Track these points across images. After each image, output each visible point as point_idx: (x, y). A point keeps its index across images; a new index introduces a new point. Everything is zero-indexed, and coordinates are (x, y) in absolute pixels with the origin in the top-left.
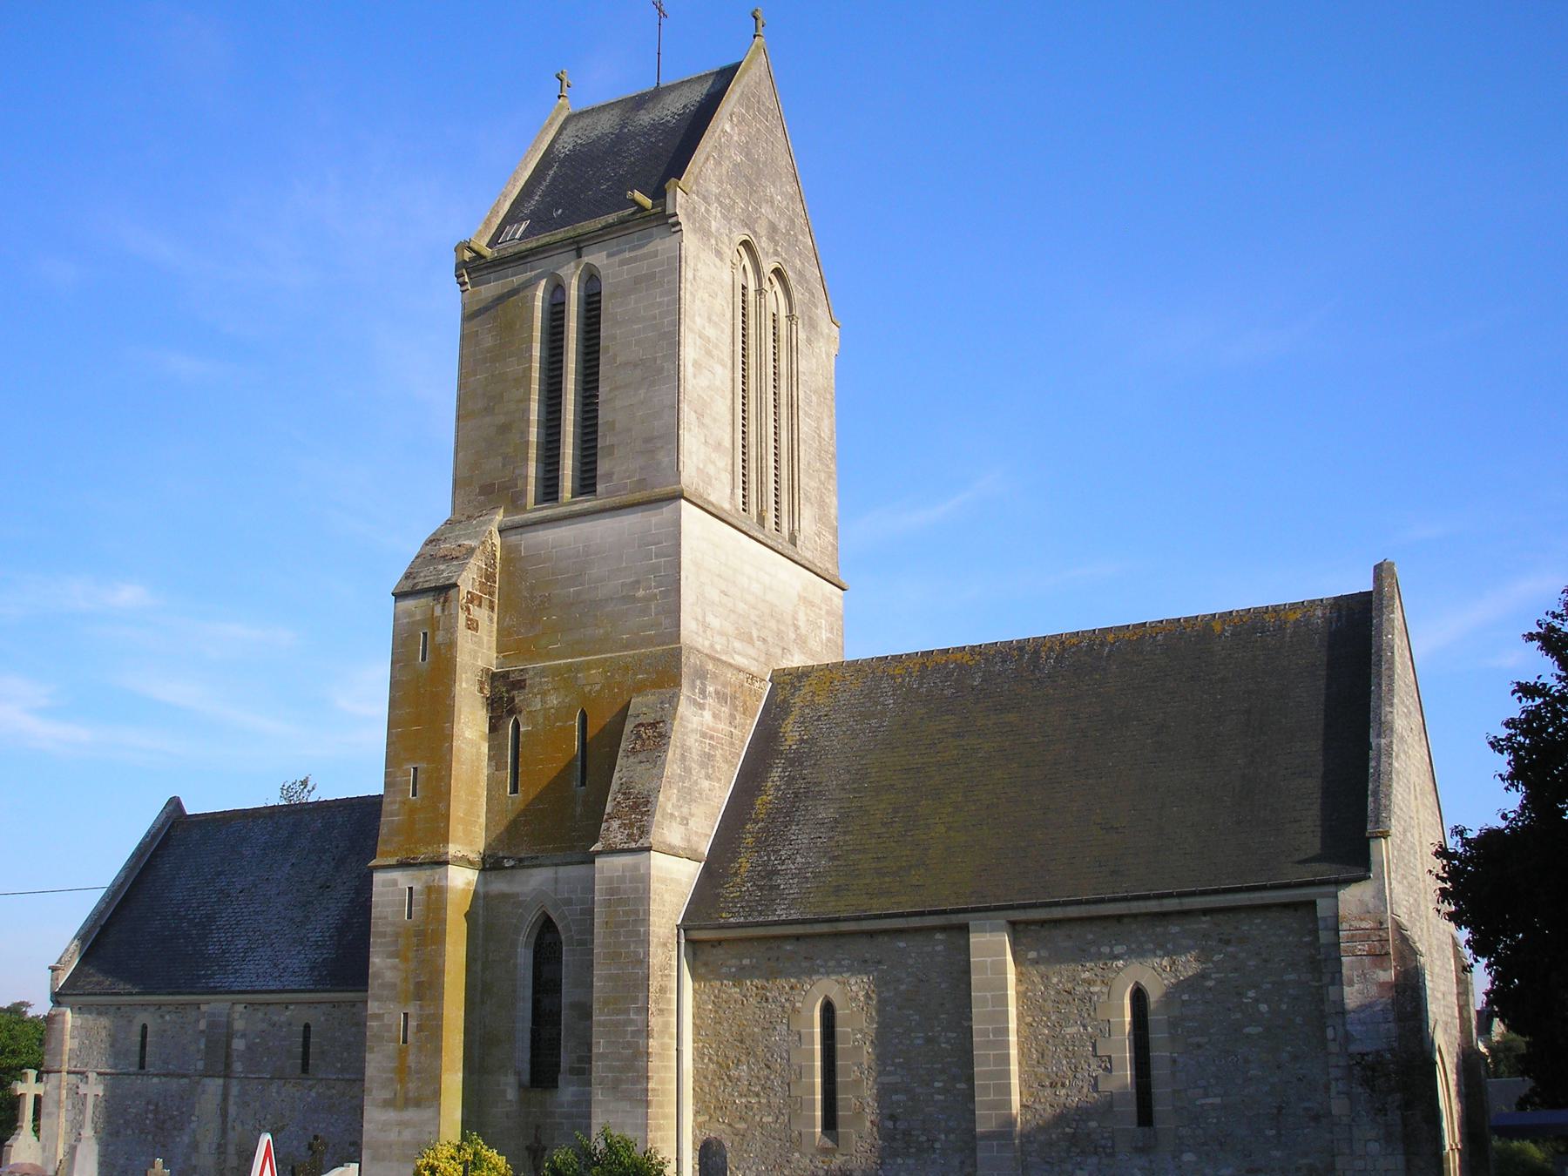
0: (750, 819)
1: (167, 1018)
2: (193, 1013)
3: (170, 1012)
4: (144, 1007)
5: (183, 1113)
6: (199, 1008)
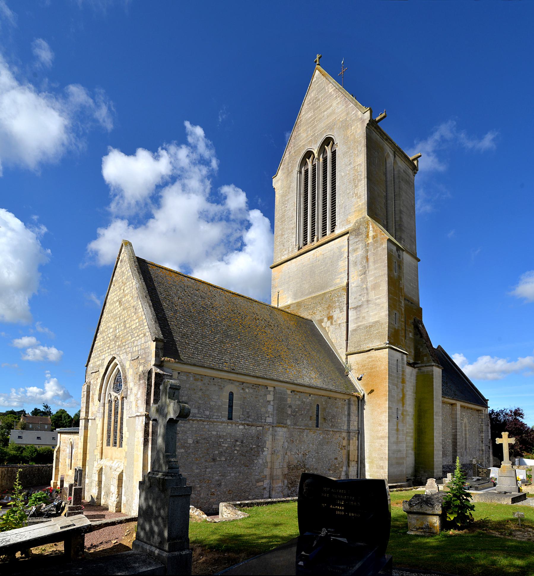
0: (497, 418)
1: (247, 390)
2: (263, 390)
3: (248, 387)
4: (231, 381)
5: (259, 446)
6: (267, 388)
